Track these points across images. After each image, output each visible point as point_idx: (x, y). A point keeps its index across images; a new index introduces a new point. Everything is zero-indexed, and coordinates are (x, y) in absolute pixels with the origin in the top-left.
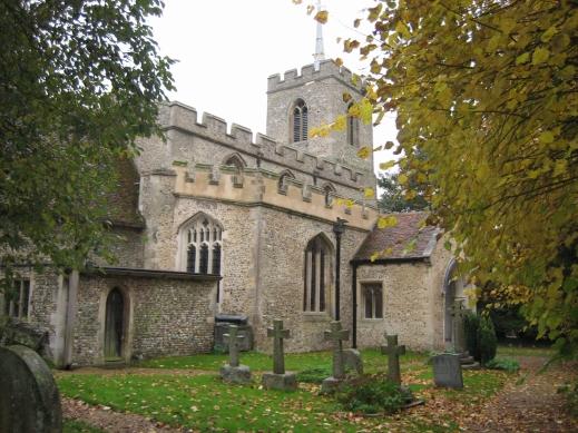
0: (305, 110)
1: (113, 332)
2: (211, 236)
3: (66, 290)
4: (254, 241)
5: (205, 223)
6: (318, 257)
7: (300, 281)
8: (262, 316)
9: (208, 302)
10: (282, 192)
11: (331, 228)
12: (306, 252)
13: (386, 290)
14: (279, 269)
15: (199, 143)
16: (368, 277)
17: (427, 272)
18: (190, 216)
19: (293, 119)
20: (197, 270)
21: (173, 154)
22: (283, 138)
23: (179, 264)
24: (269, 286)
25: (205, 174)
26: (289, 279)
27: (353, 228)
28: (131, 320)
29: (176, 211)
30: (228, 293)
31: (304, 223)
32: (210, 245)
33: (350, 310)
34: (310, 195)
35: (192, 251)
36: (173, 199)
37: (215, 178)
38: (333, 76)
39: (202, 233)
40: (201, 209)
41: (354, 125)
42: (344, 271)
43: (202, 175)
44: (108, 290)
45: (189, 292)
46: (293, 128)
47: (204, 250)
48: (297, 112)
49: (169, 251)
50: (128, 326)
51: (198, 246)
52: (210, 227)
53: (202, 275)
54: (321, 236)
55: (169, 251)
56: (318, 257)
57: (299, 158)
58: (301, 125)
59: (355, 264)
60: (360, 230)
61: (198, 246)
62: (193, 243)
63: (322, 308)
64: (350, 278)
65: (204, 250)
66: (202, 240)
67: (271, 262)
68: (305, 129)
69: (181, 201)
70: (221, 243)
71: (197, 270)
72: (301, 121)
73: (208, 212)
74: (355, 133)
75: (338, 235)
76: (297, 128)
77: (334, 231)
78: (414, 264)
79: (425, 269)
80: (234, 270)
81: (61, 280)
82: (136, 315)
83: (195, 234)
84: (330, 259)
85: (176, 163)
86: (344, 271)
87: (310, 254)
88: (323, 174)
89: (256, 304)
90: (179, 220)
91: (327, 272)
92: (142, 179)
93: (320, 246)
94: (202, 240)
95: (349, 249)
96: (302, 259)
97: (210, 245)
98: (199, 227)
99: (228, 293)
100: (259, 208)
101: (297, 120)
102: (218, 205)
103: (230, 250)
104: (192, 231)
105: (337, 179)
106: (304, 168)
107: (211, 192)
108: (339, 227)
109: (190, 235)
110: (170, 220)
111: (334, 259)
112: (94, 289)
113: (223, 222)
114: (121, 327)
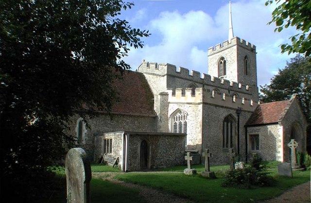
6: (229, 124)
12: (224, 122)
31: (222, 110)
32: (183, 122)
33: (244, 147)
51: (178, 122)
54: (230, 115)
56: (229, 124)
59: (246, 126)
61: (178, 122)
64: (244, 133)
73: (181, 108)
86: (242, 130)
87: (225, 123)
91: (233, 131)
97: (183, 122)
104: (175, 117)
111: (237, 125)
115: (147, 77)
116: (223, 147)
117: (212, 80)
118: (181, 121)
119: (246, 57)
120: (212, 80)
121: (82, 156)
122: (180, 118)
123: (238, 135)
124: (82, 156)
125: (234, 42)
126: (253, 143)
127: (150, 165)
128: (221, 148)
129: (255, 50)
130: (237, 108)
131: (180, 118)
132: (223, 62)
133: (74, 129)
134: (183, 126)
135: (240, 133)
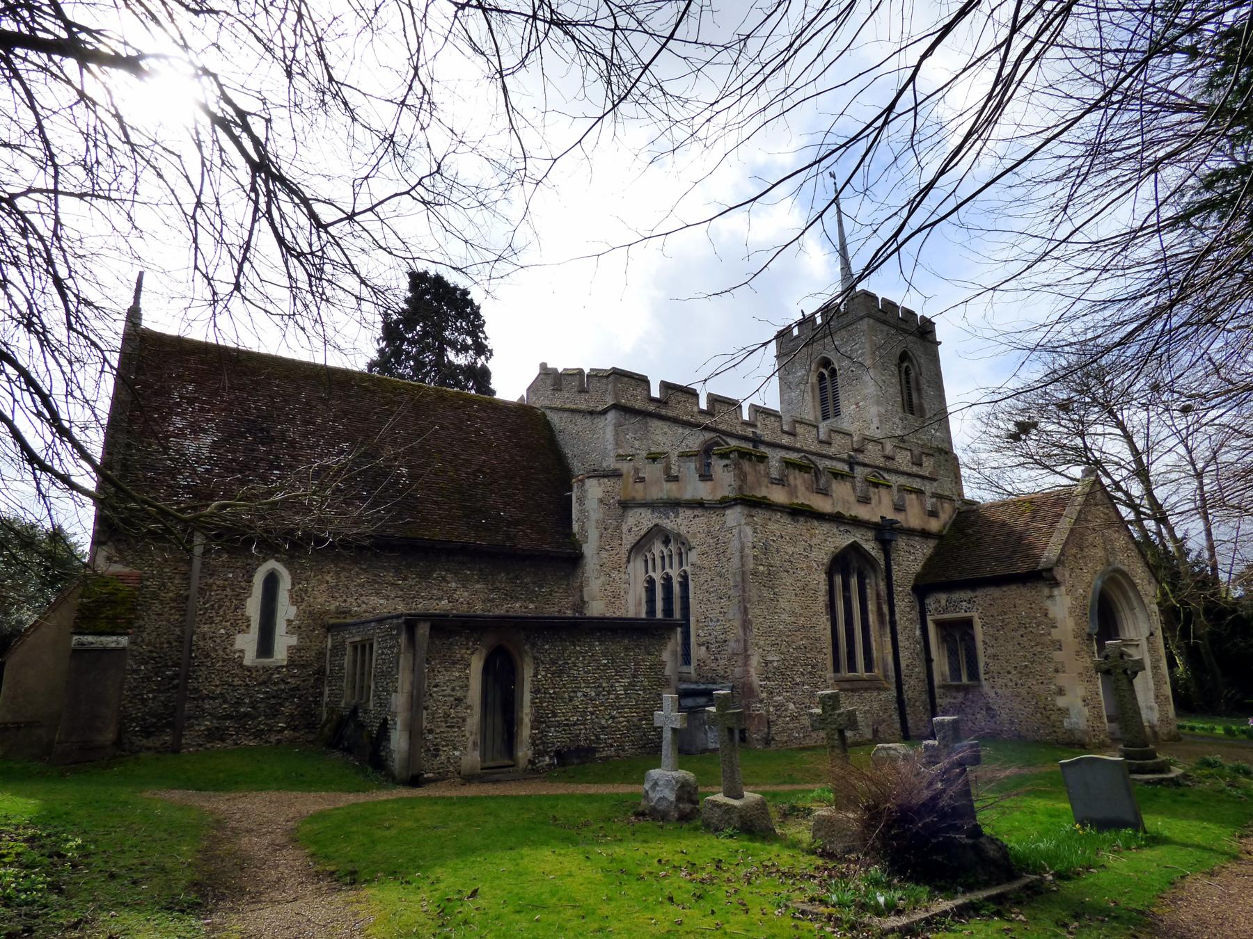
0: (833, 373)
1: (499, 720)
2: (676, 559)
3: (410, 656)
4: (736, 561)
5: (666, 542)
6: (854, 581)
7: (824, 622)
8: (755, 680)
9: (663, 664)
10: (705, 476)
11: (871, 535)
12: (830, 574)
13: (979, 632)
14: (783, 604)
15: (656, 425)
16: (945, 610)
17: (1051, 597)
18: (642, 533)
19: (817, 391)
20: (659, 615)
21: (617, 444)
22: (810, 411)
23: (633, 606)
24: (767, 634)
25: (658, 467)
26: (802, 621)
27: (910, 532)
28: (527, 697)
29: (625, 528)
30: (703, 648)
31: (822, 529)
32: (675, 573)
33: (920, 669)
34: (903, 499)
35: (651, 582)
36: (620, 511)
37: (674, 472)
38: (869, 316)
39: (663, 558)
40: (658, 521)
41: (913, 384)
42: (903, 603)
43: (653, 471)
44: (484, 653)
45: (627, 649)
46: (818, 404)
47: (668, 580)
48: (821, 377)
49: (613, 586)
50: (522, 707)
51: (657, 576)
52: (672, 546)
53: (661, 624)
54: (855, 547)
55: (613, 586)
56: (854, 581)
57: (822, 437)
58: (830, 395)
59: (922, 589)
60: (925, 534)
61: (657, 576)
62: (651, 573)
63: (869, 666)
64: (915, 615)
65: (668, 580)
66: (663, 568)
67: (767, 594)
68: (836, 399)
69: (630, 513)
70: (688, 569)
71: (659, 615)
72: (829, 389)
73: (669, 523)
74: (915, 396)
75: (886, 545)
76: (823, 401)
77: (877, 539)
78: (1024, 583)
79: (1046, 591)
80: (710, 614)
81: (403, 639)
82: (536, 691)
83: (654, 560)
84: (875, 585)
85: (621, 458)
86: (903, 603)
87: (838, 580)
88: (860, 457)
89: (746, 664)
90: (629, 540)
91: (871, 607)
92: (575, 489)
93: (855, 564)
94: (663, 568)
95: (910, 560)
96: (823, 587)
97: (675, 573)
98: (658, 548)
99: (703, 648)
100: (738, 509)
101: (823, 389)
102: (681, 510)
103: (702, 580)
104: (649, 555)
105: (889, 464)
106: (831, 451)
107: (668, 490)
108: (886, 532)
109: (646, 561)
110: (617, 542)
111: (882, 586)
112: (459, 652)
113: (689, 536)
114: (513, 713)
115: (554, 418)
116: (837, 669)
117: (655, 392)
118: (668, 570)
119: (904, 357)
120: (655, 392)
121: (426, 272)
122: (667, 560)
123: (893, 624)
124: (426, 272)
125: (112, 333)
126: (953, 655)
127: (524, 752)
128: (830, 674)
129: (932, 332)
130: (877, 519)
131: (667, 560)
132: (826, 373)
133: (241, 605)
134: (676, 588)
135: (897, 617)
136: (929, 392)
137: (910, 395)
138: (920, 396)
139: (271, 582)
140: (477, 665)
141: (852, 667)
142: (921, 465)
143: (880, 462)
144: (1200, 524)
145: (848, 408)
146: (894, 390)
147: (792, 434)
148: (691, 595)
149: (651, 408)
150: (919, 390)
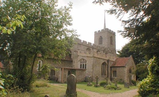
2: (85, 62)
6: (104, 66)
32: (84, 64)
35: (81, 65)
47: (83, 65)
48: (100, 38)
51: (82, 64)
54: (105, 62)
56: (104, 66)
61: (82, 64)
65: (83, 65)
84: (107, 66)
86: (109, 68)
91: (106, 68)
111: (107, 66)
136: (128, 50)
137: (111, 42)
138: (113, 42)
139: (40, 62)
140: (67, 73)
141: (103, 75)
142: (112, 51)
143: (100, 49)
144: (91, 56)
145: (103, 43)
146: (110, 41)
147: (97, 47)
148: (87, 66)
149: (81, 44)
150: (113, 41)
